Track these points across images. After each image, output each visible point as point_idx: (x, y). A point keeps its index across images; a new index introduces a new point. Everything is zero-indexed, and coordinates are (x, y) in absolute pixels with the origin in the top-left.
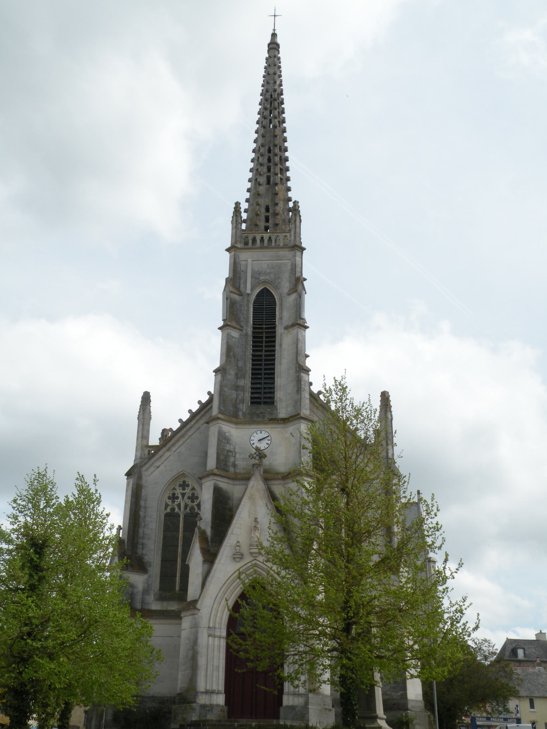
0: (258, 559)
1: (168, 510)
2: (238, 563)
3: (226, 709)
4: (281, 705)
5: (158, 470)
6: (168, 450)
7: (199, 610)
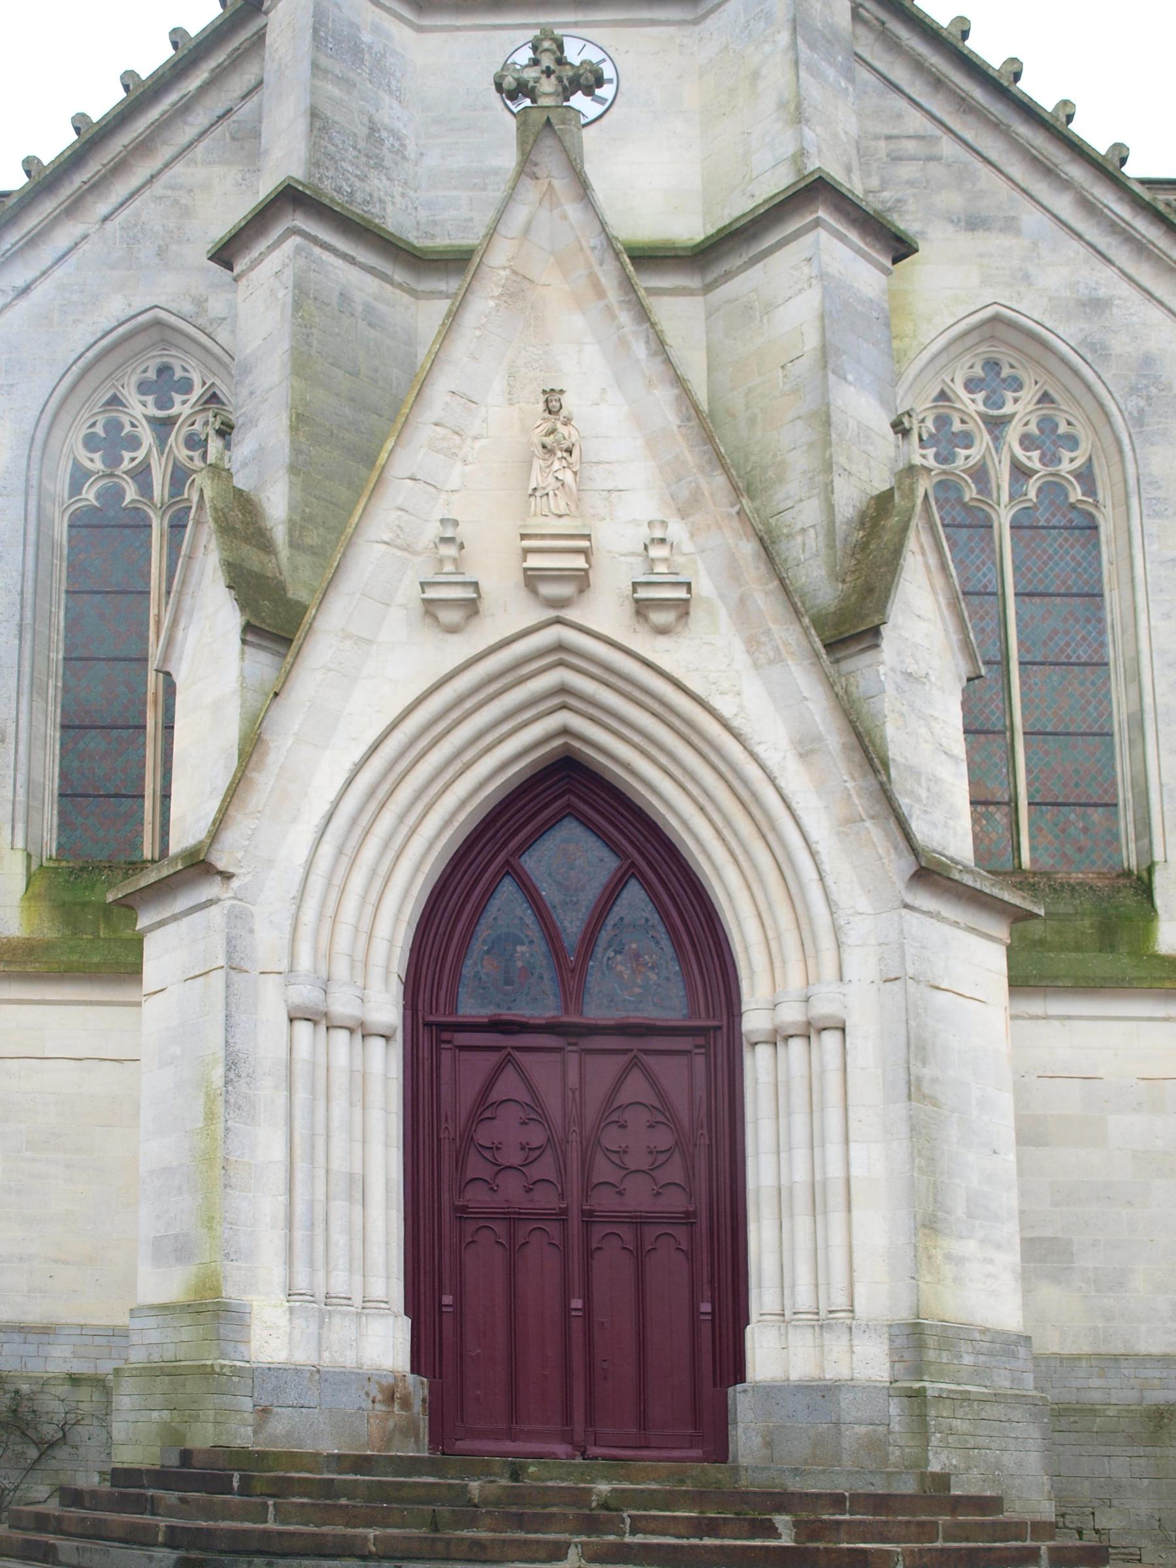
0: (570, 614)
1: (90, 495)
2: (454, 639)
3: (418, 1388)
4: (739, 1374)
5: (24, 304)
6: (72, 208)
7: (227, 876)
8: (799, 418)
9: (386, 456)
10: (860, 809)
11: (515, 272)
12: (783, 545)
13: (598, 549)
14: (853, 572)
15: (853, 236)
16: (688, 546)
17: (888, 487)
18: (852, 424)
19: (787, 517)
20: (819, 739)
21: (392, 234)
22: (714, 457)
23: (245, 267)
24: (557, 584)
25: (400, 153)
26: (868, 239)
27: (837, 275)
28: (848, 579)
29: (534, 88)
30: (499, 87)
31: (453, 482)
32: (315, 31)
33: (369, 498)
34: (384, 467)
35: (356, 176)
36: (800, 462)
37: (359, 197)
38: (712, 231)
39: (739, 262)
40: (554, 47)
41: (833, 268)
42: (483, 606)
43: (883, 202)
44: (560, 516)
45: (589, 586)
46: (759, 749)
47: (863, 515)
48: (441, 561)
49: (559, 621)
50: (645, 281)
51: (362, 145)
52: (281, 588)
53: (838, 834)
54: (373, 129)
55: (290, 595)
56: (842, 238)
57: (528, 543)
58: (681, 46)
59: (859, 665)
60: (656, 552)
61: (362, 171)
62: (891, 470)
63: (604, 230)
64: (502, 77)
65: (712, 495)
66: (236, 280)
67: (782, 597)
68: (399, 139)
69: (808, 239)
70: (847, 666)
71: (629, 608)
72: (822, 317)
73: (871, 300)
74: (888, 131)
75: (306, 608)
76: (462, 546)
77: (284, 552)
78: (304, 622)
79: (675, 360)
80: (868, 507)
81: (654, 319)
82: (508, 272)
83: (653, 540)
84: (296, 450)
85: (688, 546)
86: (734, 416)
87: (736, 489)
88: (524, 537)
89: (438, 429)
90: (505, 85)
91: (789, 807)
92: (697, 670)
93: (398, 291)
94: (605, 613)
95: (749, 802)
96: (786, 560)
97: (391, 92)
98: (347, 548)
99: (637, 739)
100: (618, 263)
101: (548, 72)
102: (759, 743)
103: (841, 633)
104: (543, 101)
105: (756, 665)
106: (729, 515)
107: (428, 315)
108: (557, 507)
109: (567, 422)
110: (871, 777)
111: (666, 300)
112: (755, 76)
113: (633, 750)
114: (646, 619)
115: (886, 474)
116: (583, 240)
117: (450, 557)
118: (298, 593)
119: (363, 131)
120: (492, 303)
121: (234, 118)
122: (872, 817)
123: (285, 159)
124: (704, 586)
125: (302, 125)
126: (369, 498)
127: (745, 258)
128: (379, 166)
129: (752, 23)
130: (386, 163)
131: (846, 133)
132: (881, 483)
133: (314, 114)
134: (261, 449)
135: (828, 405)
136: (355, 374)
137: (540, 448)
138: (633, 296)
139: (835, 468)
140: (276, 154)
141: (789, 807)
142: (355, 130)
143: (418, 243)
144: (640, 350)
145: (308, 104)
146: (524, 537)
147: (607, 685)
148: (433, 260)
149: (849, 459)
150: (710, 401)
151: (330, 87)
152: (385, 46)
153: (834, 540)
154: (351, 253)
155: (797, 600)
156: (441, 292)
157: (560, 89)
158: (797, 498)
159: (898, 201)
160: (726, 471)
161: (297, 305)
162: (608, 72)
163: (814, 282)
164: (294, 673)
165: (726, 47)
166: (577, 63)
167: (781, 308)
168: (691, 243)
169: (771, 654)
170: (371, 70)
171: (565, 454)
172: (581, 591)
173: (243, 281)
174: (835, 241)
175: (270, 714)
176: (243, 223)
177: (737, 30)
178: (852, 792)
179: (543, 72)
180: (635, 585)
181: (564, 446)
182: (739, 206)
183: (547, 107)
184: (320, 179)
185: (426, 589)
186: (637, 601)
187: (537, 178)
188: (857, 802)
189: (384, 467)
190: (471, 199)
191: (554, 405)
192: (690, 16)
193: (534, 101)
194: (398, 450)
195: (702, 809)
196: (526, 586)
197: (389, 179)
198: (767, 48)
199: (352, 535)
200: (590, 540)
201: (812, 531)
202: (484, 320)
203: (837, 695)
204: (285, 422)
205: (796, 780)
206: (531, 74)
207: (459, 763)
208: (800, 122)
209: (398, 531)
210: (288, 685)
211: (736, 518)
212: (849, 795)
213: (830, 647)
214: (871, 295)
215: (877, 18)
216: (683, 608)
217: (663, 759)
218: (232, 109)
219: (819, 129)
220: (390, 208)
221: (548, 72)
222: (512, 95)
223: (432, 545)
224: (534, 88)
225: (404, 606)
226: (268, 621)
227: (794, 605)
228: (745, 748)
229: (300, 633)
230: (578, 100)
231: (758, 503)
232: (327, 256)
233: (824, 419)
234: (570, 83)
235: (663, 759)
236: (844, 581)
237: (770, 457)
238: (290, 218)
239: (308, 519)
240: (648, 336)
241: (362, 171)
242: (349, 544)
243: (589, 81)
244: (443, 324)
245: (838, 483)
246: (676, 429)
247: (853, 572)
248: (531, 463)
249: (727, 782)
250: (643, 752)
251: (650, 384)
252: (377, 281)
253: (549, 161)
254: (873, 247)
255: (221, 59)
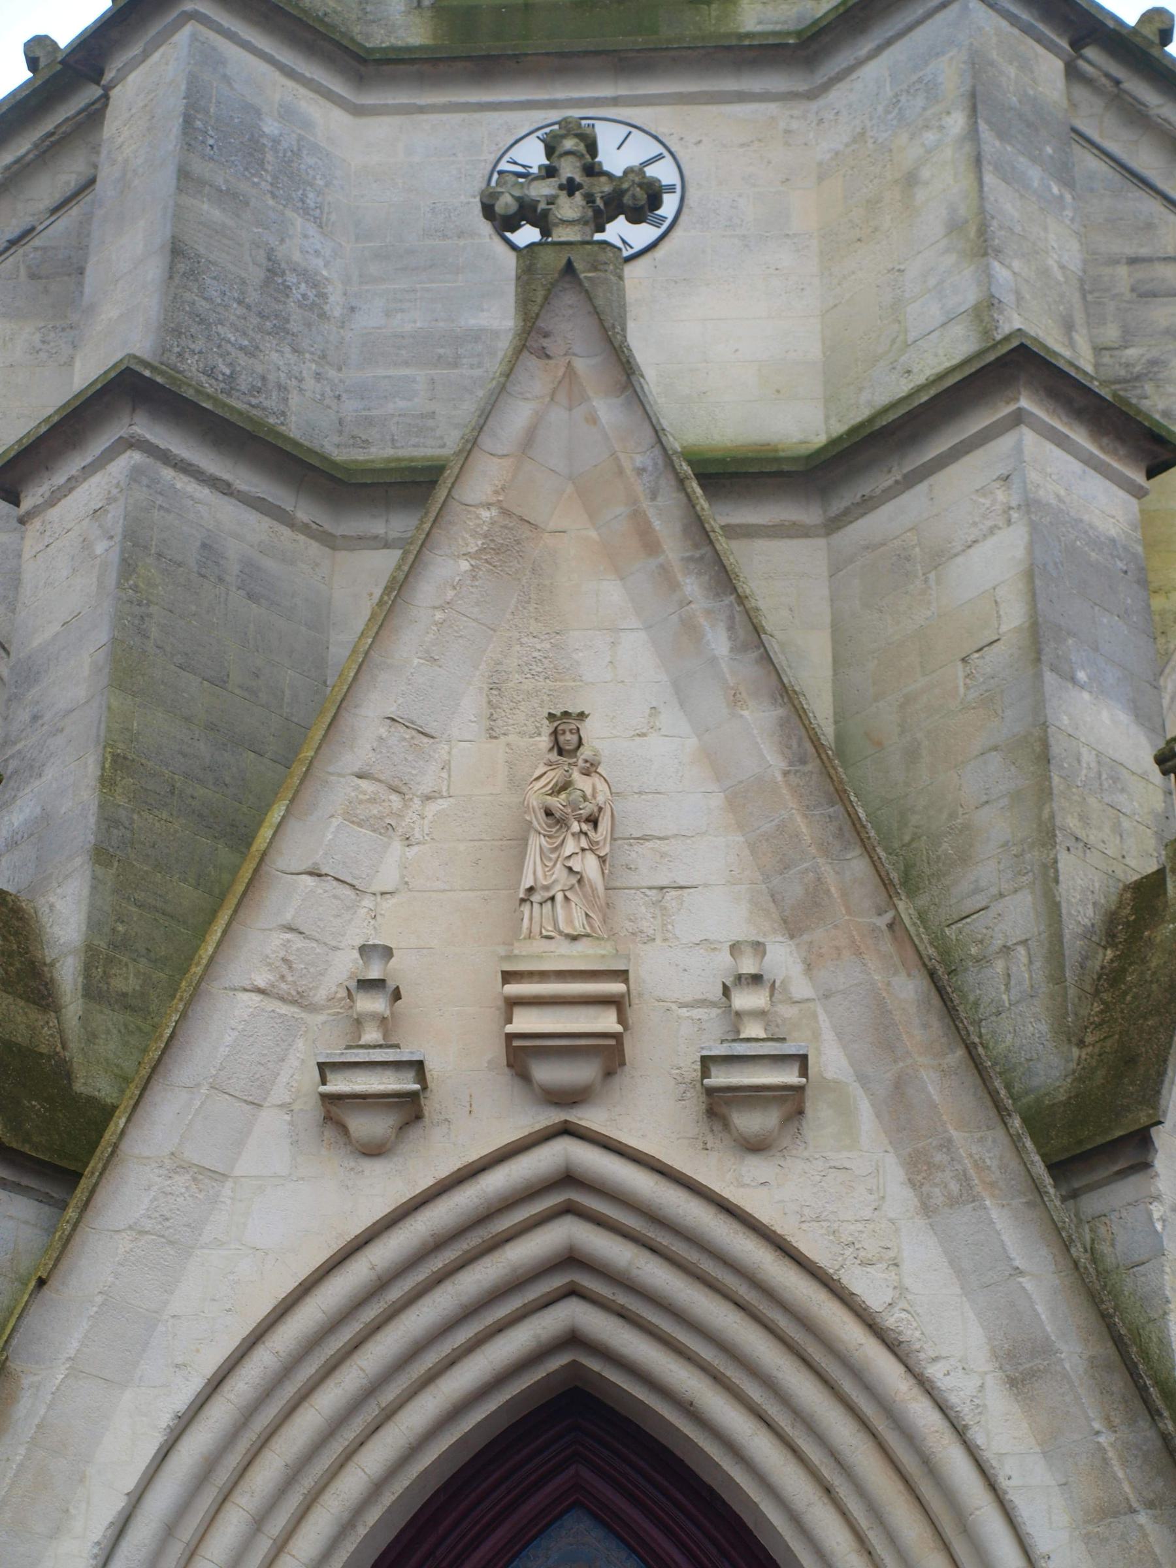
0: (591, 1118)
2: (375, 1168)
8: (995, 748)
9: (270, 833)
10: (1127, 1488)
11: (506, 512)
12: (970, 978)
13: (640, 995)
14: (1099, 1026)
15: (1080, 436)
16: (801, 988)
17: (1155, 868)
18: (1088, 757)
19: (978, 924)
20: (1045, 1349)
21: (296, 444)
22: (848, 826)
23: (40, 501)
24: (563, 1064)
25: (316, 308)
26: (1105, 441)
27: (1053, 501)
28: (1089, 1039)
29: (546, 213)
30: (488, 211)
31: (390, 885)
32: (188, 121)
33: (236, 911)
34: (264, 854)
35: (241, 348)
36: (997, 827)
37: (243, 383)
38: (839, 429)
39: (887, 481)
40: (582, 147)
41: (1048, 492)
42: (430, 1106)
43: (1127, 365)
44: (574, 938)
45: (623, 1063)
46: (935, 1372)
47: (1112, 919)
48: (358, 1022)
49: (567, 1130)
50: (724, 515)
51: (253, 296)
52: (63, 1072)
53: (1087, 1538)
54: (273, 270)
55: (79, 1087)
56: (1061, 441)
57: (514, 989)
58: (787, 132)
59: (1114, 1199)
60: (744, 1000)
61: (252, 340)
62: (1159, 835)
63: (660, 441)
64: (495, 195)
65: (844, 894)
66: (22, 521)
67: (971, 1078)
68: (315, 286)
69: (1006, 443)
70: (1093, 1203)
71: (695, 1104)
72: (1030, 575)
73: (1113, 541)
74: (1130, 250)
75: (109, 1112)
76: (397, 995)
77: (73, 1005)
78: (103, 1142)
79: (779, 659)
80: (1121, 905)
81: (744, 589)
82: (494, 512)
83: (739, 978)
84: (108, 820)
85: (801, 988)
86: (879, 745)
87: (886, 883)
88: (508, 977)
89: (364, 784)
90: (500, 208)
91: (992, 1486)
92: (817, 1219)
93: (301, 538)
94: (650, 1115)
95: (918, 1477)
96: (976, 1004)
97: (306, 211)
98: (188, 1004)
99: (707, 1353)
100: (682, 496)
101: (571, 187)
102: (935, 1360)
103: (1080, 1142)
104: (561, 234)
105: (927, 1209)
106: (874, 929)
107: (354, 577)
108: (570, 921)
109: (590, 769)
110: (1144, 1424)
111: (760, 544)
112: (911, 180)
113: (702, 1375)
114: (726, 1125)
115: (1151, 843)
116: (622, 456)
117: (373, 1016)
118: (92, 1082)
119: (256, 275)
120: (465, 565)
121: (37, 242)
122: (1150, 1505)
123: (122, 322)
124: (832, 1061)
125: (154, 270)
126: (236, 911)
127: (897, 475)
128: (281, 330)
129: (903, 98)
130: (293, 326)
131: (1062, 267)
132: (1143, 861)
133: (176, 250)
134: (45, 818)
135: (1045, 726)
136: (220, 682)
137: (541, 815)
138: (706, 550)
139: (1060, 836)
140: (109, 312)
141: (992, 1486)
142: (244, 275)
143: (340, 455)
144: (719, 642)
145: (168, 234)
146: (508, 977)
147: (654, 1250)
148: (365, 485)
149: (1084, 819)
150: (840, 717)
151: (205, 207)
152: (301, 138)
153: (1062, 967)
154: (226, 476)
155: (998, 1084)
156: (376, 537)
157: (590, 213)
158: (994, 890)
159: (1153, 362)
160: (868, 850)
161: (128, 567)
162: (663, 172)
163: (1015, 515)
164: (77, 1239)
165: (863, 134)
166: (618, 173)
167: (960, 560)
168: (804, 450)
169: (954, 1187)
170: (275, 177)
171: (585, 827)
172: (609, 1074)
173: (36, 524)
174: (1049, 447)
175: (27, 1320)
176: (43, 429)
177: (880, 108)
178: (1111, 1454)
179: (561, 187)
180: (707, 1062)
181: (584, 813)
182: (885, 388)
183: (570, 243)
184: (180, 355)
185: (330, 1076)
186: (710, 1092)
187: (548, 357)
188: (1121, 1475)
189: (264, 854)
190: (433, 381)
191: (569, 739)
192: (802, 87)
193: (545, 233)
194: (293, 824)
195: (828, 1490)
196: (510, 1065)
197: (295, 351)
198: (930, 137)
199: (201, 979)
200: (626, 981)
201: (1021, 950)
202: (450, 594)
203: (1076, 1264)
204: (92, 769)
205: (1004, 1429)
206: (541, 190)
207: (373, 1408)
208: (985, 254)
209: (284, 969)
210: (64, 1265)
211: (887, 934)
212: (1105, 1461)
213: (1059, 1168)
214: (1113, 532)
215: (1107, 75)
216: (792, 1103)
217: (755, 1393)
218: (33, 229)
219: (1017, 264)
220: (294, 399)
221: (571, 187)
222: (506, 224)
223: (343, 993)
224: (546, 213)
225: (285, 1107)
226: (35, 1139)
227: (993, 1095)
228: (909, 1369)
229: (95, 1163)
230: (618, 230)
231: (923, 901)
232: (184, 484)
233: (1038, 751)
234: (606, 204)
235: (755, 1393)
236: (1081, 1044)
237: (944, 816)
238: (126, 420)
239: (120, 944)
240: (731, 618)
241: (252, 340)
242: (196, 993)
243: (640, 199)
244: (381, 603)
245: (1067, 863)
246: (779, 778)
247: (1099, 1026)
248: (524, 841)
249: (874, 1435)
250: (717, 1378)
251: (735, 700)
252: (266, 522)
253: (569, 327)
254: (1114, 453)
255: (23, 151)
